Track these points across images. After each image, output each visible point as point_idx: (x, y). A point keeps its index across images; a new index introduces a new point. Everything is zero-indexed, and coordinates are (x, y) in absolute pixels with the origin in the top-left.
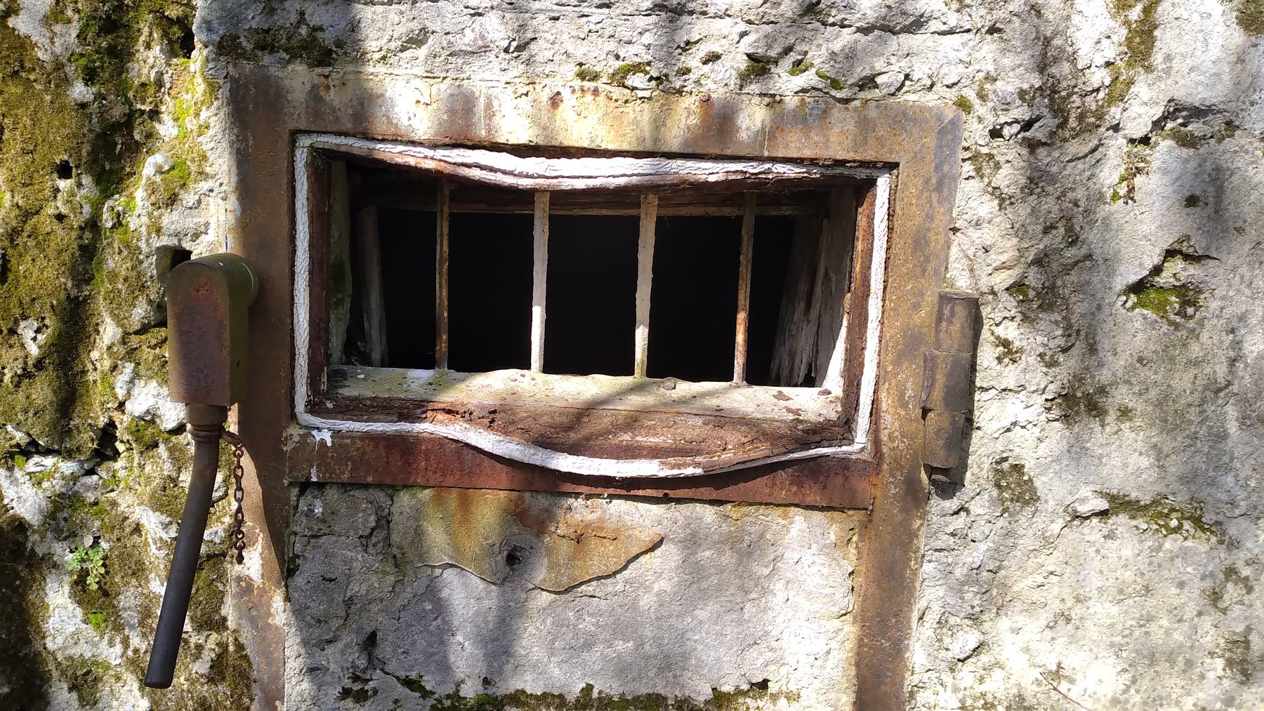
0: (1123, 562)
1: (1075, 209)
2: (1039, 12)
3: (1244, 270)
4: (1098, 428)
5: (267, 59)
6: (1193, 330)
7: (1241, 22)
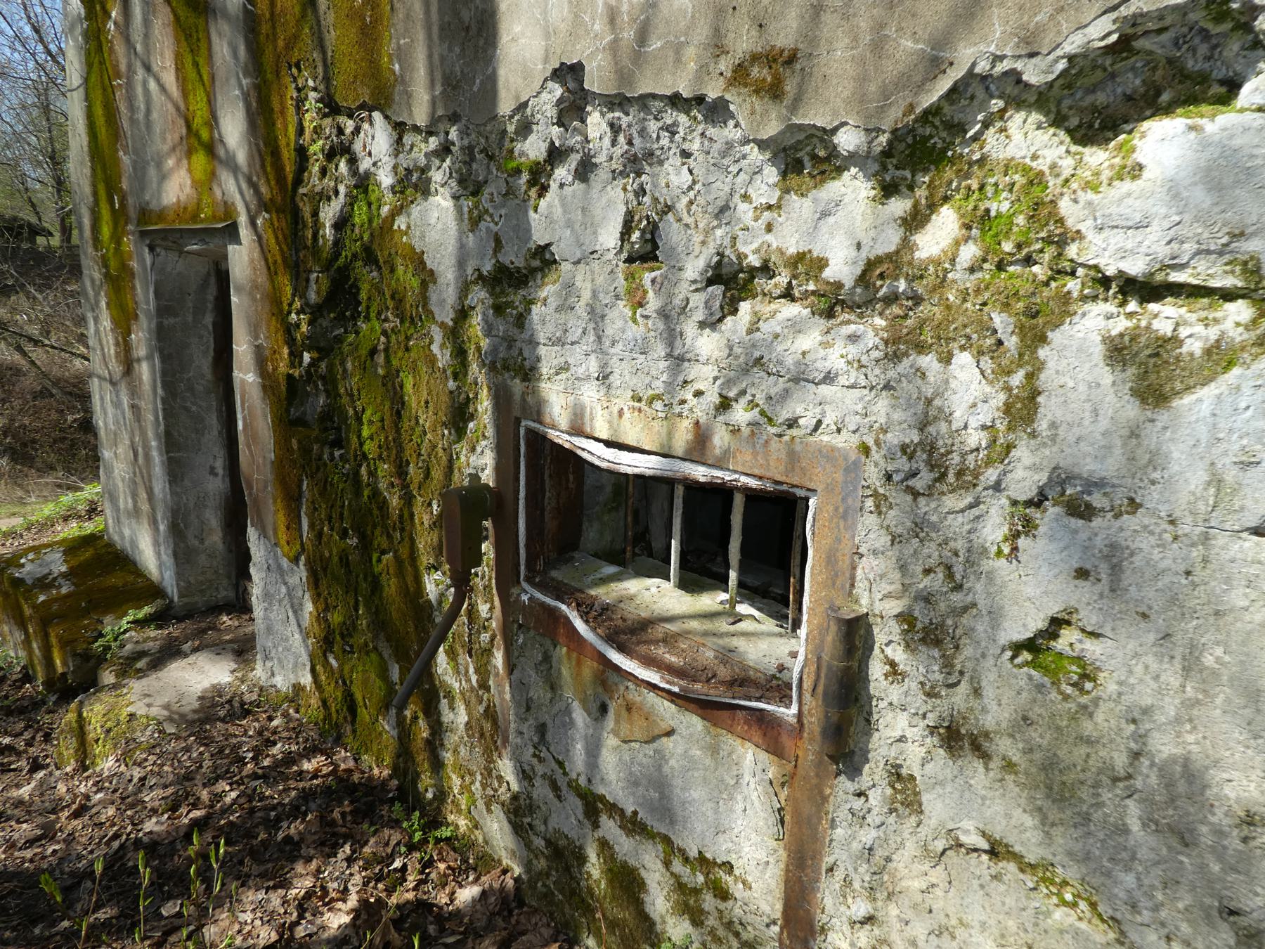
0: (1006, 908)
1: (954, 559)
2: (924, 374)
3: (1150, 659)
4: (981, 769)
5: (506, 375)
6: (1085, 707)
7: (1135, 392)
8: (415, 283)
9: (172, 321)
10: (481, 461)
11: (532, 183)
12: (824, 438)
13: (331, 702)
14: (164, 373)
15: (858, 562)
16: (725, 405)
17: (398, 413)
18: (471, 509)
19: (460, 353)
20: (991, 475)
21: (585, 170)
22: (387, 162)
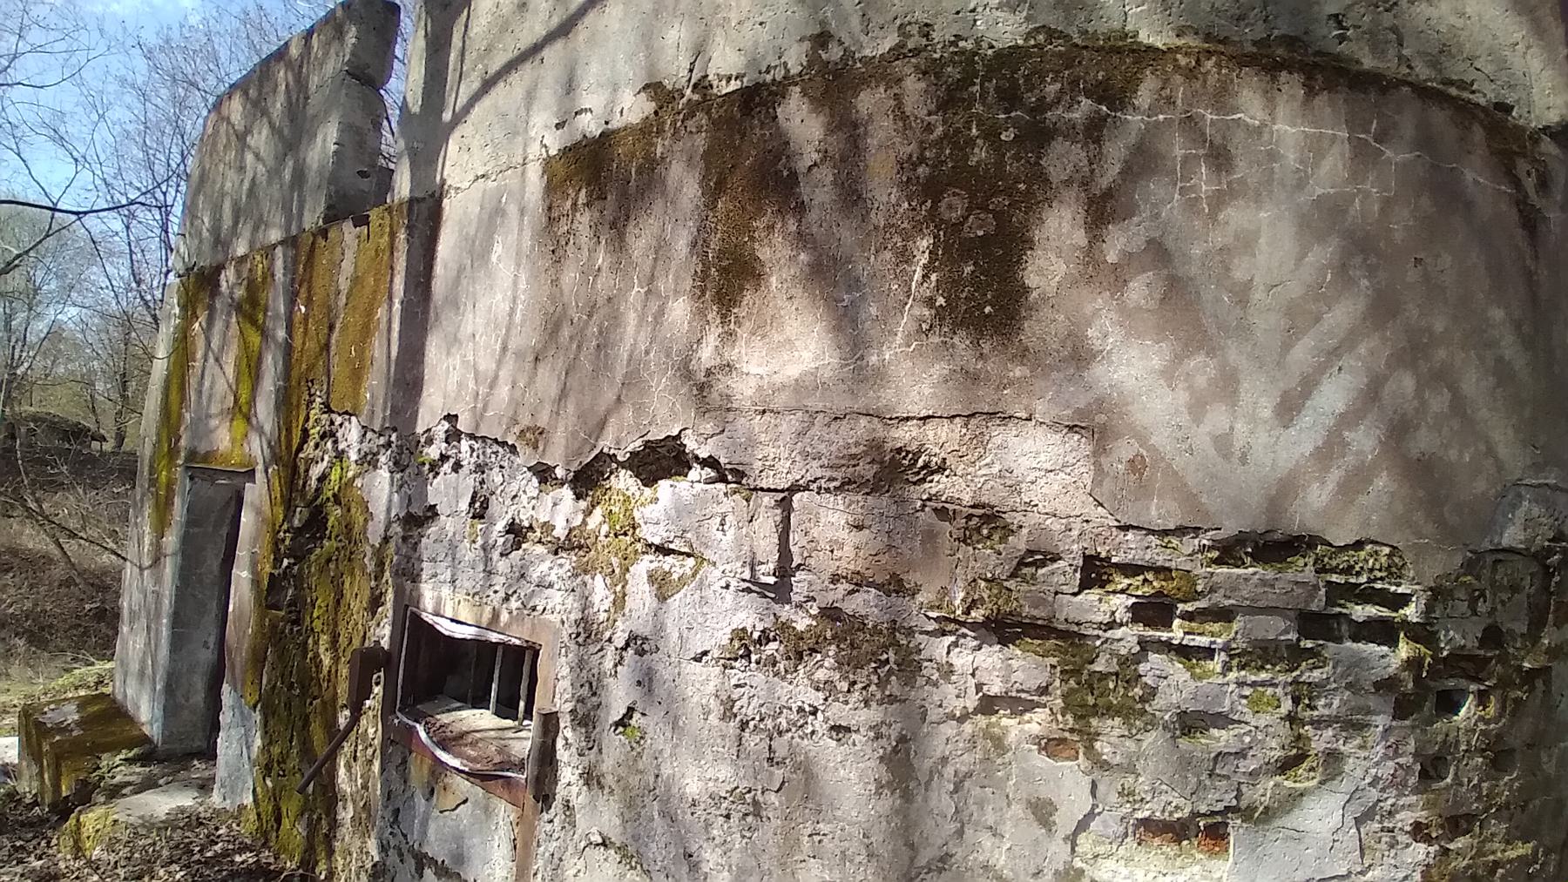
8: (361, 519)
9: (196, 530)
10: (383, 633)
11: (431, 470)
12: (547, 616)
13: (263, 816)
14: (182, 568)
15: (556, 687)
16: (507, 599)
17: (338, 602)
18: (369, 661)
19: (380, 565)
20: (607, 635)
21: (457, 467)
22: (356, 446)
